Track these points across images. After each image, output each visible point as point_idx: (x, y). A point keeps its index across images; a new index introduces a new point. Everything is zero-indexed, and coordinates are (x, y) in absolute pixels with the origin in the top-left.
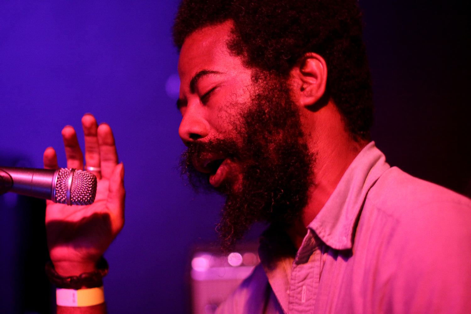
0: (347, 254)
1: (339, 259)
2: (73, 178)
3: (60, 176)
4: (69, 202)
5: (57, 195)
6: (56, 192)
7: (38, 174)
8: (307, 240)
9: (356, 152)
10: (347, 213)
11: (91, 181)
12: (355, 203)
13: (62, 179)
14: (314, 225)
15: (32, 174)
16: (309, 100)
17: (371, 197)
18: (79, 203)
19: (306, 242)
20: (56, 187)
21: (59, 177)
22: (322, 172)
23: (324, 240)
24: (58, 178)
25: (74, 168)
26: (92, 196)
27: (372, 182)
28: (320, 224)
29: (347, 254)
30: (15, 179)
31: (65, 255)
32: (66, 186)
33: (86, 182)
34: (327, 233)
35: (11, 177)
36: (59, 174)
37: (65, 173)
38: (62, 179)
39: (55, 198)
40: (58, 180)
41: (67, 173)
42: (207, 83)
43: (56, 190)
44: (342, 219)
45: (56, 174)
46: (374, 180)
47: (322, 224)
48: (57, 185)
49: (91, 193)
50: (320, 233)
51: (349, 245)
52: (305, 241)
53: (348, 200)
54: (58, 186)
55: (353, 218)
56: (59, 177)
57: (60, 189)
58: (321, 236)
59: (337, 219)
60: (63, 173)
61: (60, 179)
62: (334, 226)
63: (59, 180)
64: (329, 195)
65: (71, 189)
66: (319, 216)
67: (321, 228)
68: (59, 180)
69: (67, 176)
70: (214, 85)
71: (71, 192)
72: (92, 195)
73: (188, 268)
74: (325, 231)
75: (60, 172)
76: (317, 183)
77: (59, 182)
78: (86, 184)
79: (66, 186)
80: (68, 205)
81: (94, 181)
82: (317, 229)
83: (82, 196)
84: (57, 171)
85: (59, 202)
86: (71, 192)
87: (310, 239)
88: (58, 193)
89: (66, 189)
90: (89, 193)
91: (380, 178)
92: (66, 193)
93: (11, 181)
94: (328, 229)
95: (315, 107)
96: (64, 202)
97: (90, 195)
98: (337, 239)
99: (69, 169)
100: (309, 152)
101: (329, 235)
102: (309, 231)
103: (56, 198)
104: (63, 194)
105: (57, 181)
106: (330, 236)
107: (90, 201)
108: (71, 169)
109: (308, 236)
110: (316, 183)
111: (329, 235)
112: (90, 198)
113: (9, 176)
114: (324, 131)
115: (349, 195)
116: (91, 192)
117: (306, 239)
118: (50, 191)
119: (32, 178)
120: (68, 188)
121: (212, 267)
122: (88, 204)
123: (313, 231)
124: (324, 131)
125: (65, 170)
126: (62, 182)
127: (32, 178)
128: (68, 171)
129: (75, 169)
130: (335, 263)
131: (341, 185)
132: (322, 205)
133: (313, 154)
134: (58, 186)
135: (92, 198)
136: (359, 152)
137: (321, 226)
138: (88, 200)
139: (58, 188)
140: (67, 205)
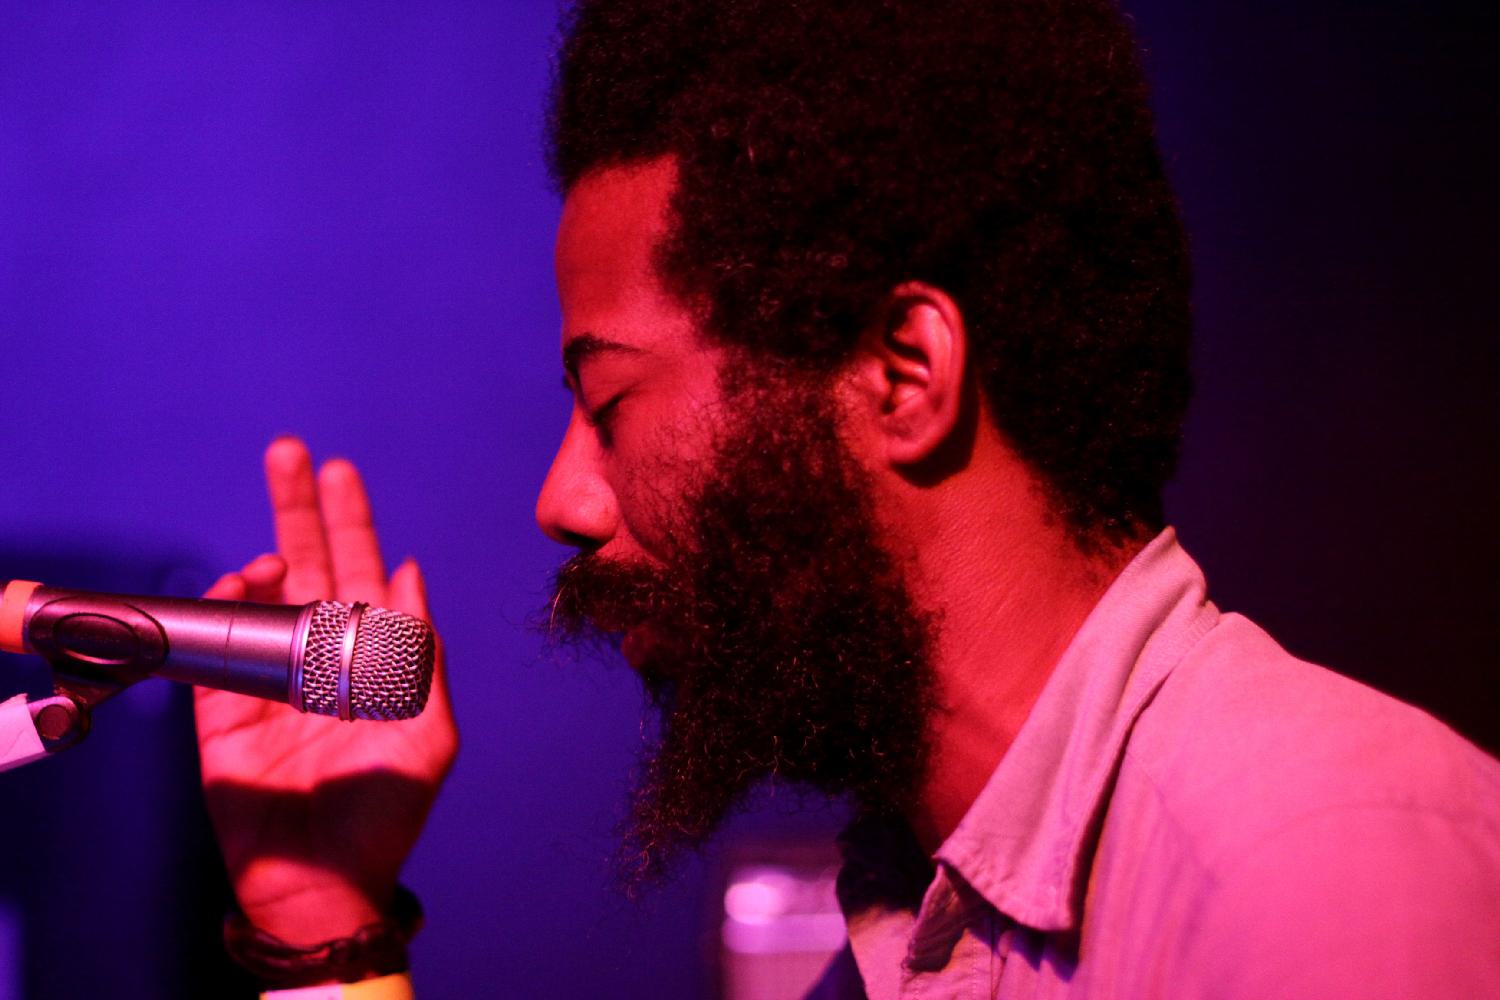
0: (1058, 948)
1: (1046, 966)
2: (358, 632)
3: (317, 626)
4: (347, 709)
5: (308, 687)
6: (304, 678)
7: (246, 620)
8: (937, 898)
9: (1095, 587)
10: (1065, 802)
11: (417, 642)
12: (1092, 765)
13: (324, 635)
14: (955, 849)
15: (228, 620)
16: (908, 449)
17: (1162, 721)
18: (377, 714)
19: (933, 905)
20: (305, 662)
21: (314, 629)
22: (967, 669)
23: (991, 895)
24: (311, 634)
25: (362, 602)
26: (418, 693)
27: (1148, 691)
28: (973, 845)
29: (1058, 948)
30: (173, 635)
31: (297, 900)
32: (335, 658)
33: (399, 646)
34: (1001, 872)
35: (160, 628)
36: (313, 621)
37: (332, 616)
38: (324, 635)
39: (300, 696)
40: (311, 638)
41: (341, 618)
42: (603, 376)
43: (306, 672)
44: (1052, 818)
45: (305, 620)
46: (1155, 684)
47: (983, 843)
48: (307, 654)
49: (414, 682)
50: (976, 874)
51: (1063, 918)
52: (931, 901)
53: (1067, 755)
54: (309, 659)
55: (1081, 817)
56: (314, 629)
57: (317, 668)
58: (978, 883)
59: (1032, 821)
60: (327, 616)
61: (317, 637)
62: (1022, 846)
63: (315, 641)
64: (1001, 743)
65: (351, 668)
66: (971, 820)
67: (980, 858)
68: (315, 641)
69: (338, 628)
70: (615, 389)
71: (351, 679)
72: (418, 688)
73: (716, 915)
74: (993, 867)
75: (316, 613)
76: (950, 705)
77: (315, 645)
78: (399, 654)
79: (337, 658)
80: (342, 719)
81: (425, 642)
82: (965, 862)
83: (373, 690)
84: (308, 614)
85: (314, 708)
86: (351, 679)
87: (944, 895)
88: (312, 681)
89: (335, 669)
90: (409, 681)
91: (1173, 676)
92: (336, 681)
93: (161, 642)
94: (1001, 861)
95: (937, 466)
96: (328, 710)
97: (412, 687)
98: (1031, 894)
99: (345, 605)
100: (917, 609)
101: (1008, 876)
102: (940, 871)
103: (305, 696)
104: (327, 683)
105: (309, 644)
106: (1011, 883)
107: (411, 707)
108: (351, 605)
109: (939, 885)
110: (946, 705)
111: (1008, 876)
112: (412, 695)
113: (154, 626)
114: (973, 537)
115: (1073, 738)
116: (417, 678)
117: (933, 895)
118: (282, 672)
119: (229, 633)
120: (344, 664)
121: (791, 911)
122: (406, 714)
123: (953, 873)
124: (973, 537)
125: (334, 606)
126: (322, 647)
127: (229, 633)
128: (344, 610)
129: (367, 605)
130: (1033, 973)
131: (1044, 711)
132: (981, 777)
133: (929, 615)
134: (309, 659)
135: (417, 697)
136: (1106, 587)
137: (977, 852)
138: (404, 702)
139: (310, 665)
140: (337, 719)
